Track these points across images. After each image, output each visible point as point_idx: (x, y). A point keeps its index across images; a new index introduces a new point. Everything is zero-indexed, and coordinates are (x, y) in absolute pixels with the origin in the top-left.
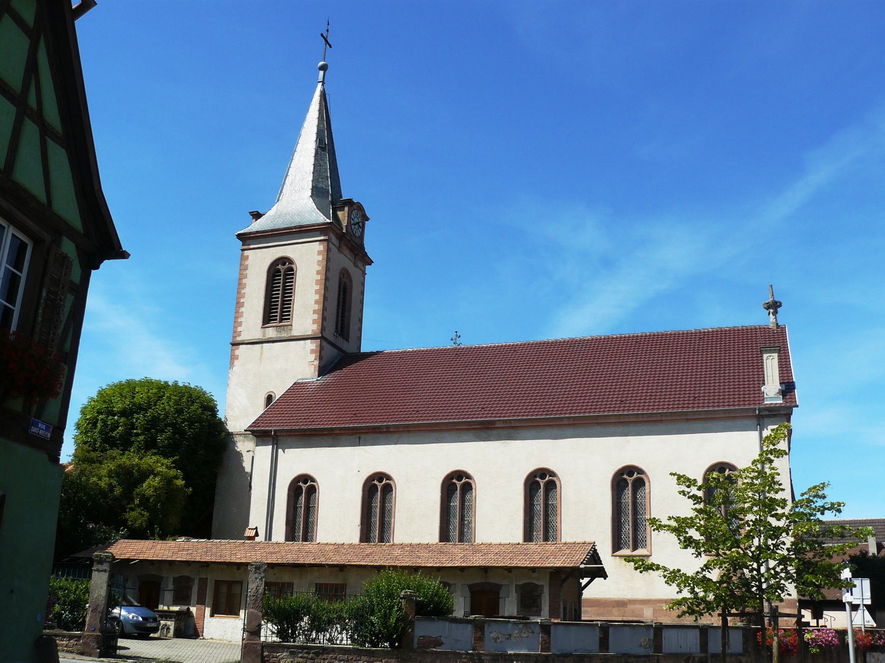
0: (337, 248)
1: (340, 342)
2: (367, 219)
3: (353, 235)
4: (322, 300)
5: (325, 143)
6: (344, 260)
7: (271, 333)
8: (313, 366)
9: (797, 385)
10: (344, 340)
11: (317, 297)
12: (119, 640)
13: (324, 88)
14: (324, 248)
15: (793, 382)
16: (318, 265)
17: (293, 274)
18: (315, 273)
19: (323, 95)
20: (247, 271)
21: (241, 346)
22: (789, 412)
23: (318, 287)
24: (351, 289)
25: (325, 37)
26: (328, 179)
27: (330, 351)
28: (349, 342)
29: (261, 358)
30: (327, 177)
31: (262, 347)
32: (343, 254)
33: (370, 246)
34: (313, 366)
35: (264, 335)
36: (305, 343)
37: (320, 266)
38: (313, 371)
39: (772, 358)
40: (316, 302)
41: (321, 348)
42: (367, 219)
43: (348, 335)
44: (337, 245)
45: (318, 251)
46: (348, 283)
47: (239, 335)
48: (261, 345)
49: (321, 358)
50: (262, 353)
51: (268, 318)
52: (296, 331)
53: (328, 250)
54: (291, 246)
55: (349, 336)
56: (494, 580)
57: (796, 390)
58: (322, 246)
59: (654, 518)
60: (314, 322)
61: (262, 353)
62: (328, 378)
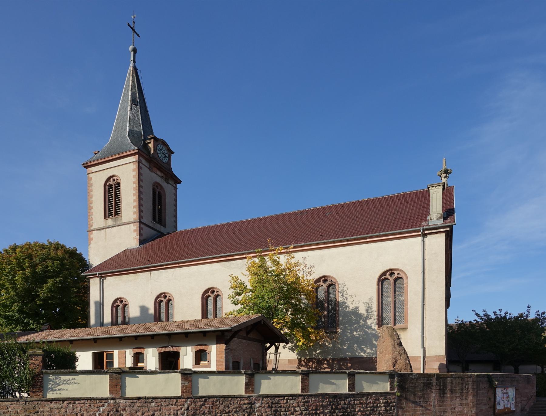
0: (148, 168)
1: (158, 227)
2: (173, 153)
3: (160, 160)
4: (138, 199)
5: (137, 101)
6: (156, 177)
7: (110, 222)
8: (136, 239)
9: (456, 211)
10: (162, 227)
11: (135, 198)
12: (269, 345)
13: (135, 66)
14: (136, 167)
15: (454, 209)
16: (133, 178)
17: (119, 186)
18: (132, 183)
19: (135, 70)
20: (92, 187)
21: (94, 232)
22: (453, 211)
23: (134, 192)
24: (165, 196)
25: (132, 27)
26: (140, 125)
27: (148, 232)
28: (166, 228)
29: (105, 239)
30: (140, 124)
31: (106, 231)
32: (154, 172)
33: (176, 169)
34: (136, 239)
35: (106, 224)
36: (130, 227)
37: (135, 178)
38: (136, 242)
39: (436, 192)
40: (135, 201)
41: (140, 229)
42: (173, 153)
43: (165, 224)
44: (148, 166)
45: (133, 169)
46: (162, 192)
47: (92, 226)
48: (104, 230)
49: (140, 234)
50: (106, 235)
51: (108, 214)
52: (124, 220)
53: (140, 168)
54: (116, 167)
55: (165, 224)
56: (163, 371)
57: (455, 214)
58: (135, 166)
59: (488, 315)
60: (134, 213)
61: (106, 235)
62: (143, 246)
